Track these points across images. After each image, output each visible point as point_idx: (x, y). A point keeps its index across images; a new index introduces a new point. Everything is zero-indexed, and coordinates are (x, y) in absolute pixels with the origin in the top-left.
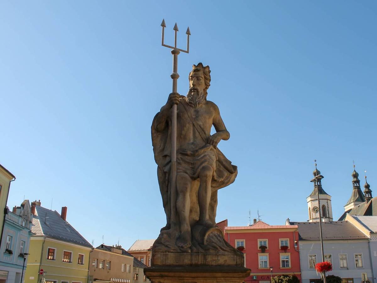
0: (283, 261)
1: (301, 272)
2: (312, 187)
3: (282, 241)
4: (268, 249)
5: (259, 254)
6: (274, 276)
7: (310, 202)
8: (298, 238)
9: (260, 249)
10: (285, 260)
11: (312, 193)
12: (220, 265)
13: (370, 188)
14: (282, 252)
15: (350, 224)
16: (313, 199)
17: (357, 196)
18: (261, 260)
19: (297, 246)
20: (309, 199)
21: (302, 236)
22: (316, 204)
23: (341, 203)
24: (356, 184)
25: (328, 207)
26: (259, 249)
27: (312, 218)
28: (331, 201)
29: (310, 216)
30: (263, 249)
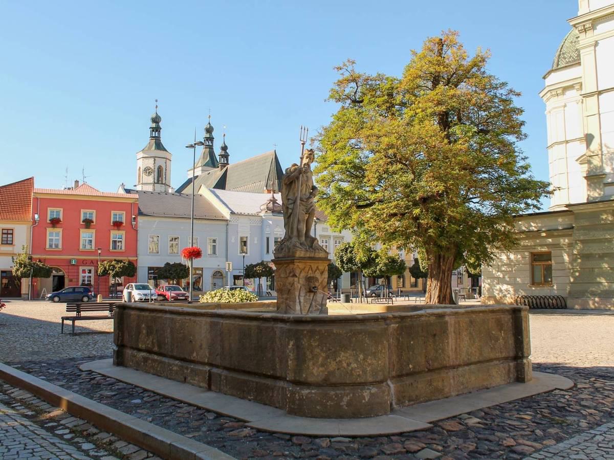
0: (115, 242)
1: (137, 257)
2: (145, 138)
3: (115, 215)
4: (94, 224)
5: (82, 230)
6: (103, 261)
7: (142, 159)
8: (137, 212)
9: (84, 223)
10: (117, 240)
11: (146, 147)
12: (320, 258)
13: (227, 151)
14: (114, 229)
15: (205, 199)
16: (147, 156)
17: (207, 158)
18: (83, 239)
19: (135, 223)
20: (141, 155)
21: (143, 210)
22: (150, 163)
23: (183, 166)
24: (209, 142)
25: (166, 170)
26: (81, 223)
27: (141, 182)
28: (171, 161)
29: (139, 179)
30: (88, 223)
